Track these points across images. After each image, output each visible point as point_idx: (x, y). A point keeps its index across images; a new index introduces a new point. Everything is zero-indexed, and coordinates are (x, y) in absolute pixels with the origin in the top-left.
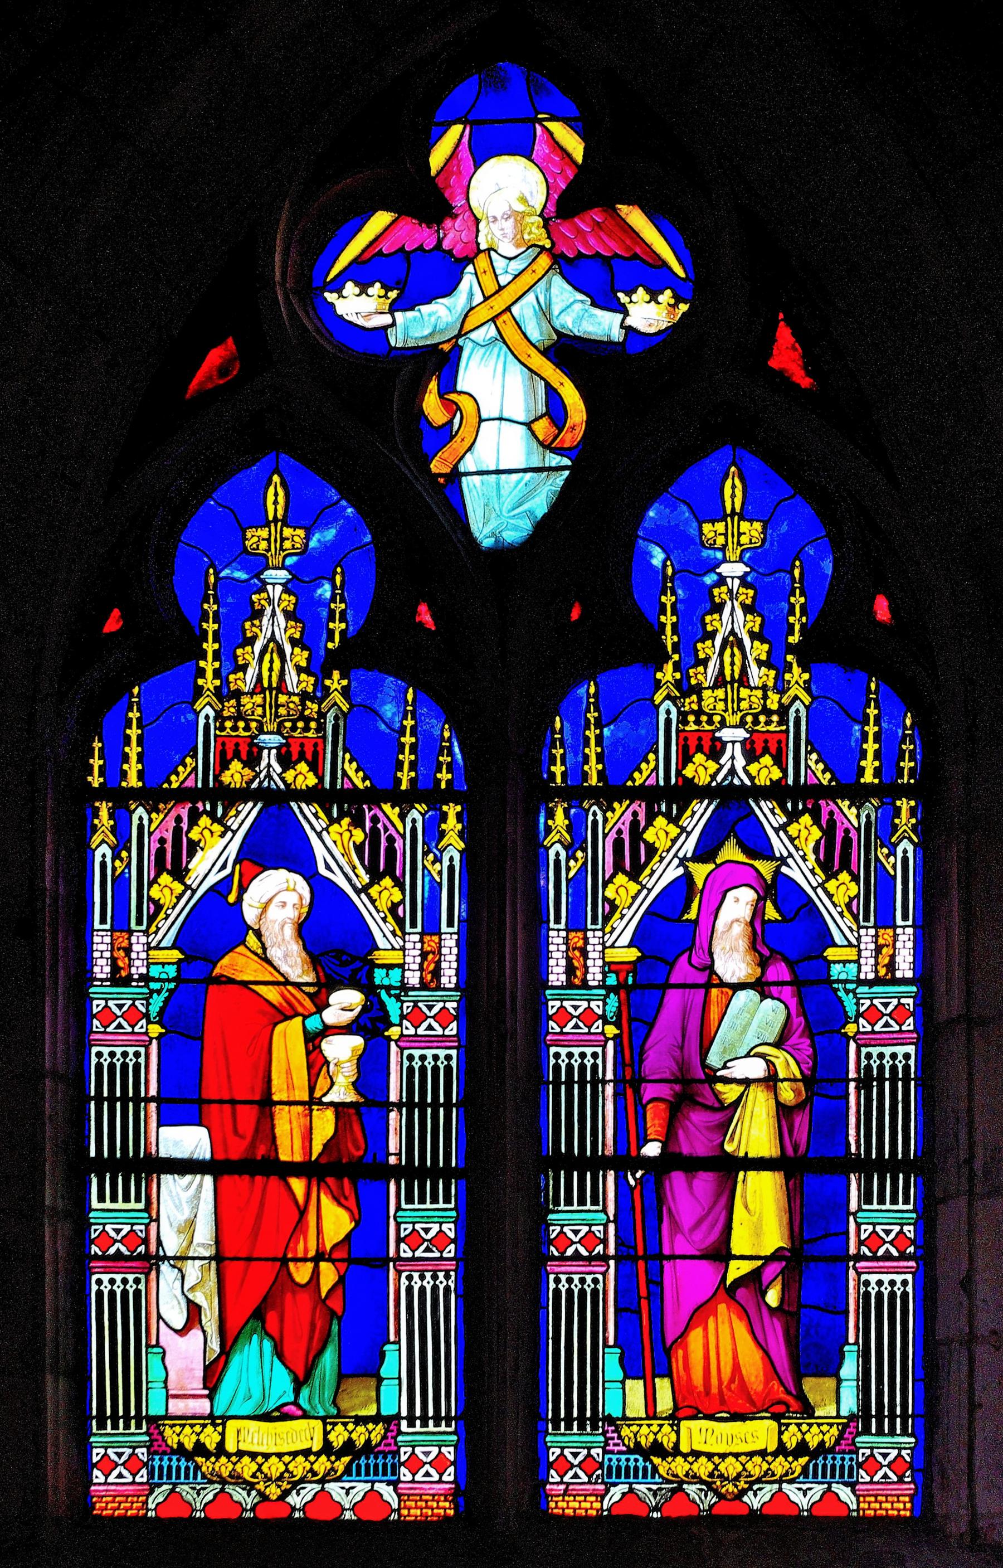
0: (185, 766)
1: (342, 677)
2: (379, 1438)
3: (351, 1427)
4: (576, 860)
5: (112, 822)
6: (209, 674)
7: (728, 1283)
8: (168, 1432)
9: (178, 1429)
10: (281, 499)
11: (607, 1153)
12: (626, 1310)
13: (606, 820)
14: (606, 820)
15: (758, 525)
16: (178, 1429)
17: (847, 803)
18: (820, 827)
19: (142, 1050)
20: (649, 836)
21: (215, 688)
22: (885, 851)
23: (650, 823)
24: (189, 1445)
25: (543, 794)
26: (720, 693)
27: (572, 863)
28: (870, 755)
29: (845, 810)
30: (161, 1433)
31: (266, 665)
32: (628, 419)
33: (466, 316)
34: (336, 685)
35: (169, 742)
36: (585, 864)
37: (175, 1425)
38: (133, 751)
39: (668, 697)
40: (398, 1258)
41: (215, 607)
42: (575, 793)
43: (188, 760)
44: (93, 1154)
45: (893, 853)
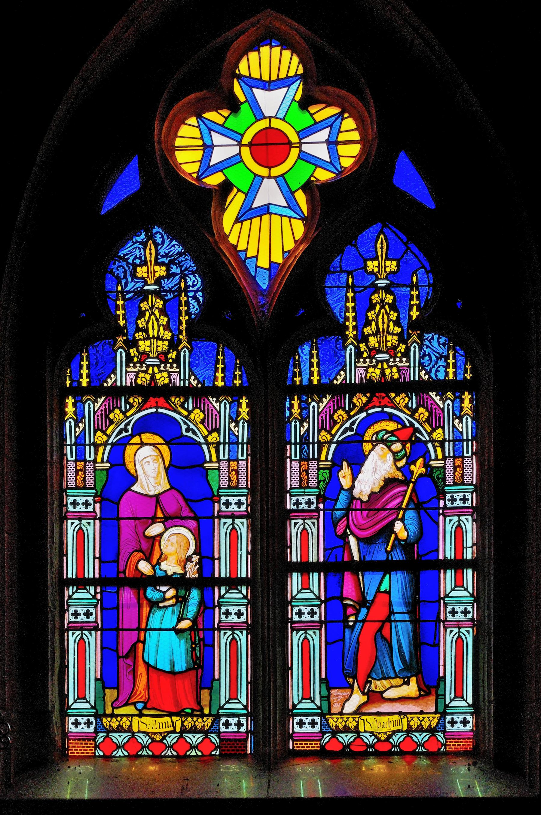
0: (111, 379)
2: (209, 725)
3: (205, 719)
4: (79, 428)
6: (351, 329)
10: (385, 245)
13: (94, 407)
14: (94, 407)
15: (394, 263)
17: (434, 393)
19: (315, 521)
24: (115, 726)
25: (65, 392)
26: (148, 343)
27: (77, 429)
28: (85, 376)
29: (434, 397)
32: (338, 211)
34: (351, 335)
35: (104, 366)
38: (85, 372)
39: (352, 343)
40: (446, 620)
42: (78, 392)
43: (112, 376)
44: (322, 574)
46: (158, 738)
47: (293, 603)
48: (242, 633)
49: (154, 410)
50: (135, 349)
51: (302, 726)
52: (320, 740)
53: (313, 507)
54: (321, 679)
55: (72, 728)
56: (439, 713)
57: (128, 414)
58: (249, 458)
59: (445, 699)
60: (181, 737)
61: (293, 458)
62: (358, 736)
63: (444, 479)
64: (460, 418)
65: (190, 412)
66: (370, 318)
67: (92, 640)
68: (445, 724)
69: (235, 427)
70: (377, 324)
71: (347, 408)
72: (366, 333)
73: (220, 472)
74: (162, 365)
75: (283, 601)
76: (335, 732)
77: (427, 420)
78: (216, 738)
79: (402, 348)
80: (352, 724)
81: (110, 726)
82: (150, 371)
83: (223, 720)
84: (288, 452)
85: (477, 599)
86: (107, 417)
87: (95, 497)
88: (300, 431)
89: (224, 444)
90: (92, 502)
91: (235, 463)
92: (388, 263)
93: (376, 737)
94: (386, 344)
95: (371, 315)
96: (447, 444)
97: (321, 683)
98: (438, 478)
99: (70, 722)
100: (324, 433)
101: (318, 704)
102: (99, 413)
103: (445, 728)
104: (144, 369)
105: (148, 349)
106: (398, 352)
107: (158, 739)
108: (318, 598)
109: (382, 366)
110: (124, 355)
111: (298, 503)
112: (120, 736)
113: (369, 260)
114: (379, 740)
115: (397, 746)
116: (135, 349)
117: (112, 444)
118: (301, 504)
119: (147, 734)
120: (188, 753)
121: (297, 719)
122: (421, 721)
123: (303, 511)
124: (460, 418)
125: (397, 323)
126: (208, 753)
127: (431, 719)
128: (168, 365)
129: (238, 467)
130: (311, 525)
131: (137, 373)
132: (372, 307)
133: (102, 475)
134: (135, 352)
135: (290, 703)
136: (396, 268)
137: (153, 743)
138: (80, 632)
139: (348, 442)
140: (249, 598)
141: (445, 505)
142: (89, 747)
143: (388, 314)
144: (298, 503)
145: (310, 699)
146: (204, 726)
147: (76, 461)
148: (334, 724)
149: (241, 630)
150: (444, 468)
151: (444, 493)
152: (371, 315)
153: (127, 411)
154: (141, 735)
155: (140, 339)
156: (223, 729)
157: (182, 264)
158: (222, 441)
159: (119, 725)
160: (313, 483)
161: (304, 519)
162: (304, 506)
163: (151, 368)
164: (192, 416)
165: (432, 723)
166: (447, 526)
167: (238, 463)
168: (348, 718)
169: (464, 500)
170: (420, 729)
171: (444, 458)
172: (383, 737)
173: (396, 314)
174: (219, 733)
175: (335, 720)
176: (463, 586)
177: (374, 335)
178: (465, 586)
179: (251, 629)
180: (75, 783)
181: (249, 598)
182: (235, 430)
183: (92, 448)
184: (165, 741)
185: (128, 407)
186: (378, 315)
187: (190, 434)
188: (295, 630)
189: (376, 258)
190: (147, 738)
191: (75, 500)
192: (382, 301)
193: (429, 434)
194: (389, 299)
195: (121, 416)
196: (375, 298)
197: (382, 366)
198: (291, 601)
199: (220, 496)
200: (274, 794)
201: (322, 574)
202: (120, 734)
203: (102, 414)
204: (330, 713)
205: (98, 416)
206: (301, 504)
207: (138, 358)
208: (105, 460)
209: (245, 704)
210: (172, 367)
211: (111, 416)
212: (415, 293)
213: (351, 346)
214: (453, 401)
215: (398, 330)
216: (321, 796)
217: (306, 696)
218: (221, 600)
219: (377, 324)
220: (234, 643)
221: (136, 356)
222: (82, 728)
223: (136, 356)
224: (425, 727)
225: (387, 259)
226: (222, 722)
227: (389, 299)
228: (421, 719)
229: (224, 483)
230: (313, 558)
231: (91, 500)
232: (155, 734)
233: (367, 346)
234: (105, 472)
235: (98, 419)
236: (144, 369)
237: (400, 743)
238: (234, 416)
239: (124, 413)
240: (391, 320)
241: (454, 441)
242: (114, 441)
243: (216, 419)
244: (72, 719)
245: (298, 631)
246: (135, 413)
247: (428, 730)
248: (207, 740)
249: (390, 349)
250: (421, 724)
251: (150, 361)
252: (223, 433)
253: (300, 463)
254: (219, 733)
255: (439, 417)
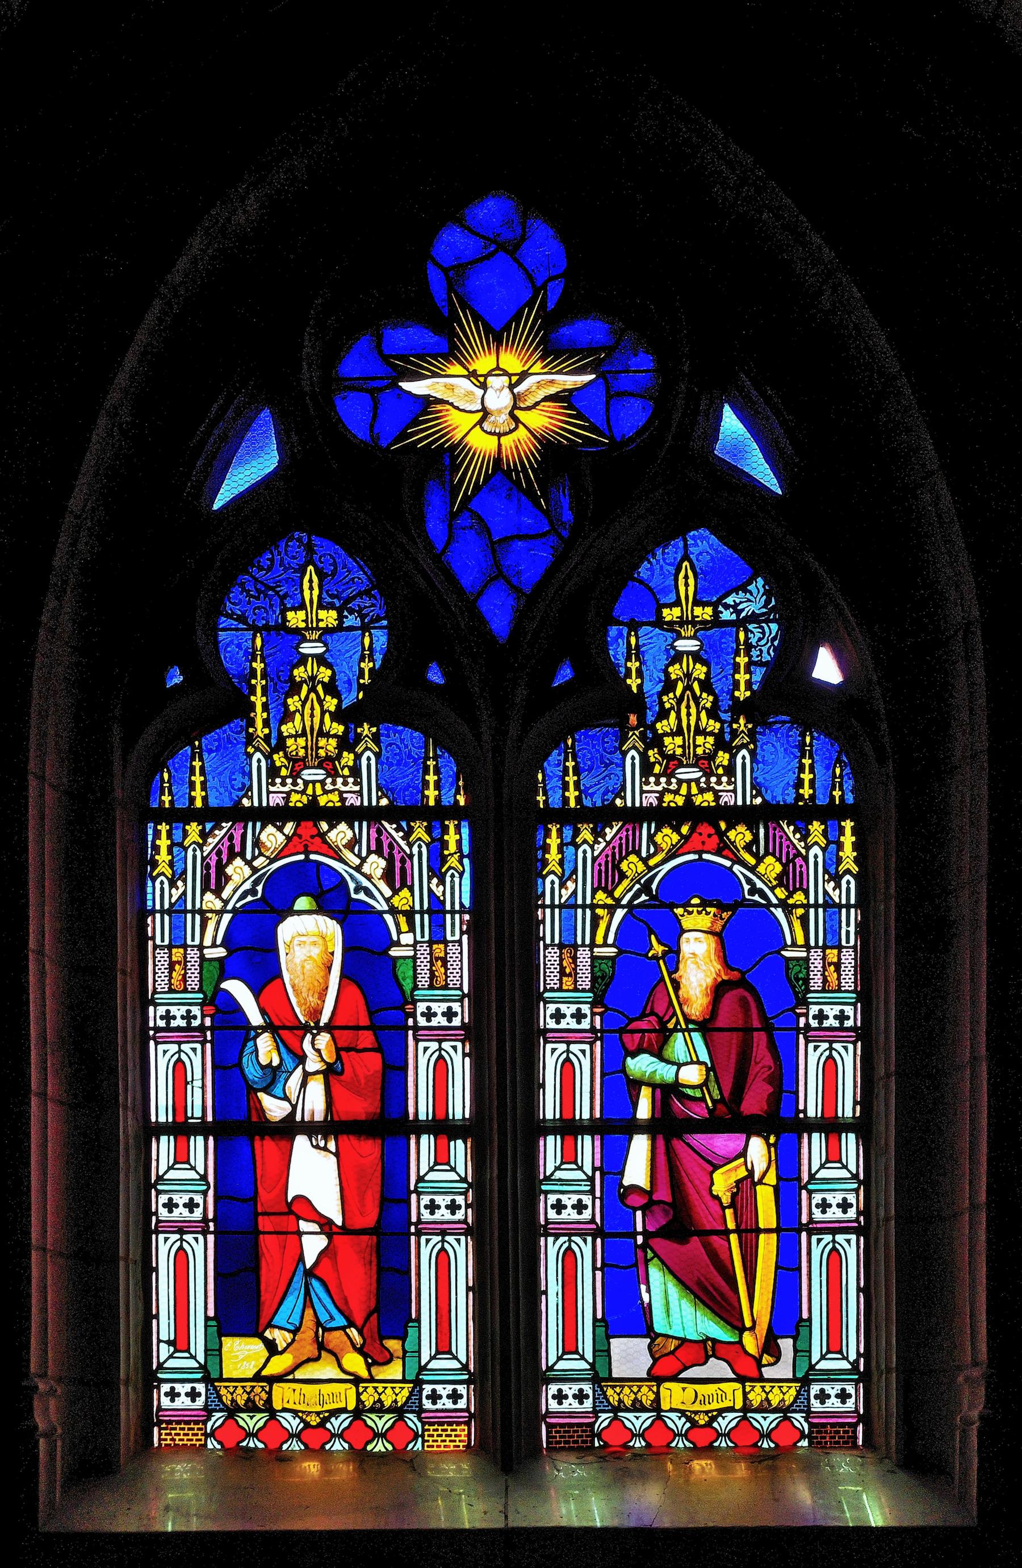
1: (748, 722)
2: (404, 1399)
4: (177, 888)
5: (855, 854)
7: (338, 1221)
8: (610, 1392)
9: (618, 1390)
11: (160, 1120)
12: (781, 1268)
16: (618, 1390)
18: (781, 863)
19: (587, 1047)
20: (229, 870)
21: (749, 730)
22: (832, 884)
23: (230, 861)
24: (628, 1402)
30: (604, 1393)
31: (684, 711)
33: (375, 414)
36: (575, 892)
37: (616, 1386)
41: (262, 665)
45: (838, 886)
46: (314, 1420)
47: (159, 1187)
48: (585, 1241)
49: (302, 857)
50: (281, 753)
51: (563, 1401)
52: (205, 1423)
53: (196, 1023)
54: (595, 1319)
55: (166, 1402)
56: (409, 1382)
57: (652, 862)
58: (465, 937)
59: (810, 1357)
60: (745, 1418)
61: (158, 942)
62: (659, 1418)
63: (807, 980)
64: (837, 878)
65: (760, 860)
66: (292, 708)
67: (199, 1249)
68: (420, 1399)
69: (834, 889)
70: (679, 718)
71: (249, 856)
72: (660, 732)
73: (415, 962)
74: (329, 780)
75: (532, 1185)
76: (232, 1411)
77: (779, 877)
78: (415, 1420)
79: (723, 758)
80: (647, 1396)
81: (620, 1401)
82: (684, 791)
83: (427, 1389)
84: (150, 929)
85: (867, 1182)
86: (616, 867)
87: (202, 1005)
88: (171, 896)
89: (422, 912)
90: (588, 1013)
91: (181, 950)
92: (322, 614)
93: (689, 1419)
94: (694, 751)
95: (293, 703)
96: (417, 917)
97: (594, 1327)
98: (797, 979)
99: (550, 1394)
100: (209, 896)
101: (202, 1362)
102: (602, 860)
103: (809, 1406)
104: (674, 786)
105: (302, 753)
106: (719, 766)
107: (314, 1423)
108: (204, 1177)
109: (689, 788)
110: (263, 764)
111: (168, 1017)
112: (765, 1418)
113: (290, 609)
114: (307, 1425)
115: (639, 1435)
116: (281, 753)
117: (234, 910)
118: (174, 1018)
119: (295, 1413)
120: (369, 1448)
121: (553, 1389)
122: (380, 1394)
123: (831, 1029)
124: (837, 878)
125: (712, 714)
126: (233, 1445)
127: (785, 1390)
128: (340, 780)
129: (446, 953)
130: (580, 1055)
131: (662, 794)
132: (295, 688)
133: (211, 968)
134: (283, 760)
135: (155, 1360)
136: (335, 623)
137: (696, 1430)
138: (439, 1238)
139: (248, 912)
140: (470, 1180)
141: (807, 1024)
142: (197, 1435)
143: (697, 700)
144: (168, 1017)
145: (840, 1352)
146: (396, 1401)
147: (431, 943)
148: (230, 1397)
149: (582, 1235)
150: (807, 960)
151: (807, 1004)
152: (293, 703)
153: (650, 856)
154: (288, 1416)
155: (666, 734)
156: (427, 1404)
157: (740, 607)
158: (417, 907)
159: (636, 1399)
160: (193, 983)
161: (179, 1043)
162: (831, 1022)
163: (684, 786)
164: (761, 869)
165: (786, 1397)
166: (421, 1058)
167: (186, 950)
168: (253, 1387)
169: (449, 1014)
170: (378, 1408)
171: (807, 946)
172: (314, 1420)
173: (335, 701)
174: (808, 1413)
175: (231, 1390)
176: (840, 1161)
177: (672, 734)
178: (844, 1161)
179: (474, 1231)
180: (178, 1499)
181: (470, 1180)
182: (438, 891)
183: (198, 917)
184: (715, 1425)
185: (652, 850)
186: (679, 701)
187: (362, 896)
188: (551, 1235)
189: (302, 606)
190: (683, 1420)
191: (429, 1008)
192: (688, 675)
193: (388, 900)
194: (325, 674)
195: (641, 867)
196: (299, 673)
197: (689, 788)
198: (156, 1183)
199: (414, 1002)
200: (517, 1521)
201: (211, 1138)
202: (765, 1415)
203: (607, 862)
204: (221, 1379)
205: (600, 865)
206: (827, 1017)
207: (287, 769)
208: (219, 942)
209: (464, 1362)
210: (345, 783)
211: (624, 866)
212: (258, 666)
213: (633, 752)
214: (824, 850)
215: (714, 726)
216: (599, 1525)
217: (570, 1347)
218: (420, 1185)
219: (679, 718)
220: (835, 1256)
221: (285, 766)
222: (183, 1402)
223: (285, 766)
224: (387, 1403)
225: (320, 607)
226: (425, 1393)
227: (700, 671)
228: (231, 1390)
229: (424, 981)
230: (584, 1111)
231: (586, 1009)
232: (696, 1413)
233: (661, 753)
234: (216, 964)
235: (600, 871)
236: (674, 786)
237: (731, 1430)
238: (832, 870)
239: (645, 861)
240: (704, 708)
241: (170, 912)
242: (238, 905)
243: (801, 873)
244: (165, 1388)
245: (557, 1236)
246: (664, 861)
247: (393, 1409)
248: (230, 1422)
249: (702, 758)
250: (767, 1399)
251: (307, 774)
252: (425, 895)
253: (824, 952)
254: (808, 1413)
255: (801, 873)
